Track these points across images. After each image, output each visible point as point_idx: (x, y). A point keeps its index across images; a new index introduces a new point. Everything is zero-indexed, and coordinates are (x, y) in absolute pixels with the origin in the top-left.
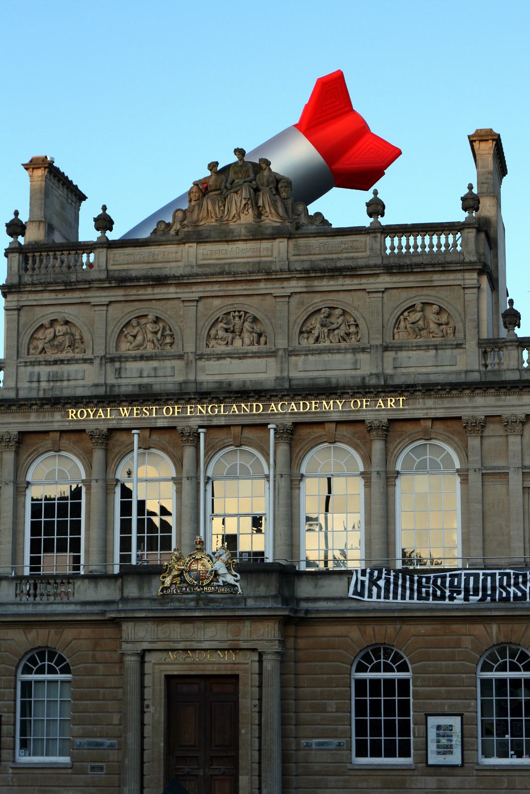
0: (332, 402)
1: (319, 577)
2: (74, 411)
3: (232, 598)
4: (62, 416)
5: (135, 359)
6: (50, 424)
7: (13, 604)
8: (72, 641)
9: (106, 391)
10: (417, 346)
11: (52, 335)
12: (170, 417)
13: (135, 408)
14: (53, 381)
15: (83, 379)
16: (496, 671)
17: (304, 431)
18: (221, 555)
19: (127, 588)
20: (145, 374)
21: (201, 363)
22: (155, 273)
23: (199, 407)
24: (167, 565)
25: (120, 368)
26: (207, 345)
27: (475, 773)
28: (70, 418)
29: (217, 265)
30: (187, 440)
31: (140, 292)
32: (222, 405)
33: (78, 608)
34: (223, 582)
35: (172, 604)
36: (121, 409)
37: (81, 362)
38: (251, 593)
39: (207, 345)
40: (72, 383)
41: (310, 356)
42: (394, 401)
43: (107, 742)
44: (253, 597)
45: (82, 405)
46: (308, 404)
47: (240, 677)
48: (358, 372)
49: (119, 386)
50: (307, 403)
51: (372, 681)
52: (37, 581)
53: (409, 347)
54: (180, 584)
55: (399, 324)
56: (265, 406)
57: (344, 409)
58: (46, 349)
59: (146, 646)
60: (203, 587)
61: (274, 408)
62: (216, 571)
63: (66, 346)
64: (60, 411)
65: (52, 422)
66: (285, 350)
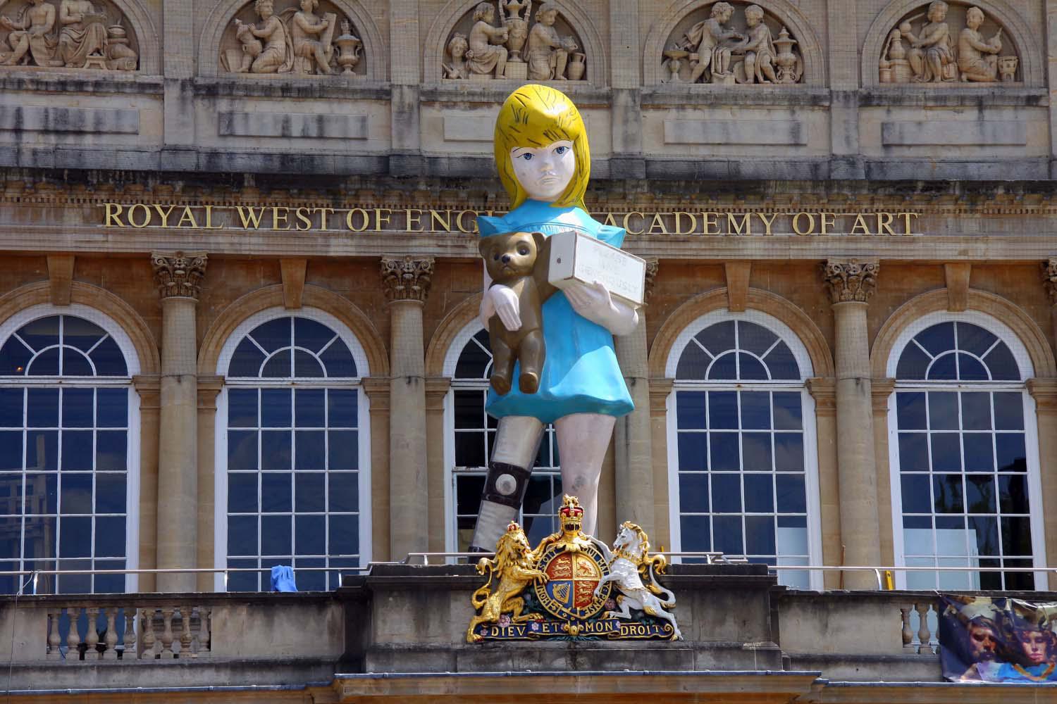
1: (831, 606)
4: (86, 220)
5: (268, 92)
6: (54, 237)
7: (43, 669)
9: (198, 165)
10: (936, 99)
11: (51, 19)
13: (275, 209)
14: (57, 132)
15: (136, 133)
19: (384, 622)
20: (296, 130)
21: (429, 113)
23: (434, 213)
24: (487, 567)
30: (408, 291)
35: (510, 663)
36: (240, 209)
37: (128, 90)
38: (703, 638)
40: (105, 140)
42: (891, 219)
44: (711, 648)
48: (801, 154)
49: (231, 155)
53: (918, 99)
54: (522, 614)
55: (889, 49)
58: (34, 54)
60: (582, 622)
63: (91, 50)
65: (59, 232)
66: (632, 92)
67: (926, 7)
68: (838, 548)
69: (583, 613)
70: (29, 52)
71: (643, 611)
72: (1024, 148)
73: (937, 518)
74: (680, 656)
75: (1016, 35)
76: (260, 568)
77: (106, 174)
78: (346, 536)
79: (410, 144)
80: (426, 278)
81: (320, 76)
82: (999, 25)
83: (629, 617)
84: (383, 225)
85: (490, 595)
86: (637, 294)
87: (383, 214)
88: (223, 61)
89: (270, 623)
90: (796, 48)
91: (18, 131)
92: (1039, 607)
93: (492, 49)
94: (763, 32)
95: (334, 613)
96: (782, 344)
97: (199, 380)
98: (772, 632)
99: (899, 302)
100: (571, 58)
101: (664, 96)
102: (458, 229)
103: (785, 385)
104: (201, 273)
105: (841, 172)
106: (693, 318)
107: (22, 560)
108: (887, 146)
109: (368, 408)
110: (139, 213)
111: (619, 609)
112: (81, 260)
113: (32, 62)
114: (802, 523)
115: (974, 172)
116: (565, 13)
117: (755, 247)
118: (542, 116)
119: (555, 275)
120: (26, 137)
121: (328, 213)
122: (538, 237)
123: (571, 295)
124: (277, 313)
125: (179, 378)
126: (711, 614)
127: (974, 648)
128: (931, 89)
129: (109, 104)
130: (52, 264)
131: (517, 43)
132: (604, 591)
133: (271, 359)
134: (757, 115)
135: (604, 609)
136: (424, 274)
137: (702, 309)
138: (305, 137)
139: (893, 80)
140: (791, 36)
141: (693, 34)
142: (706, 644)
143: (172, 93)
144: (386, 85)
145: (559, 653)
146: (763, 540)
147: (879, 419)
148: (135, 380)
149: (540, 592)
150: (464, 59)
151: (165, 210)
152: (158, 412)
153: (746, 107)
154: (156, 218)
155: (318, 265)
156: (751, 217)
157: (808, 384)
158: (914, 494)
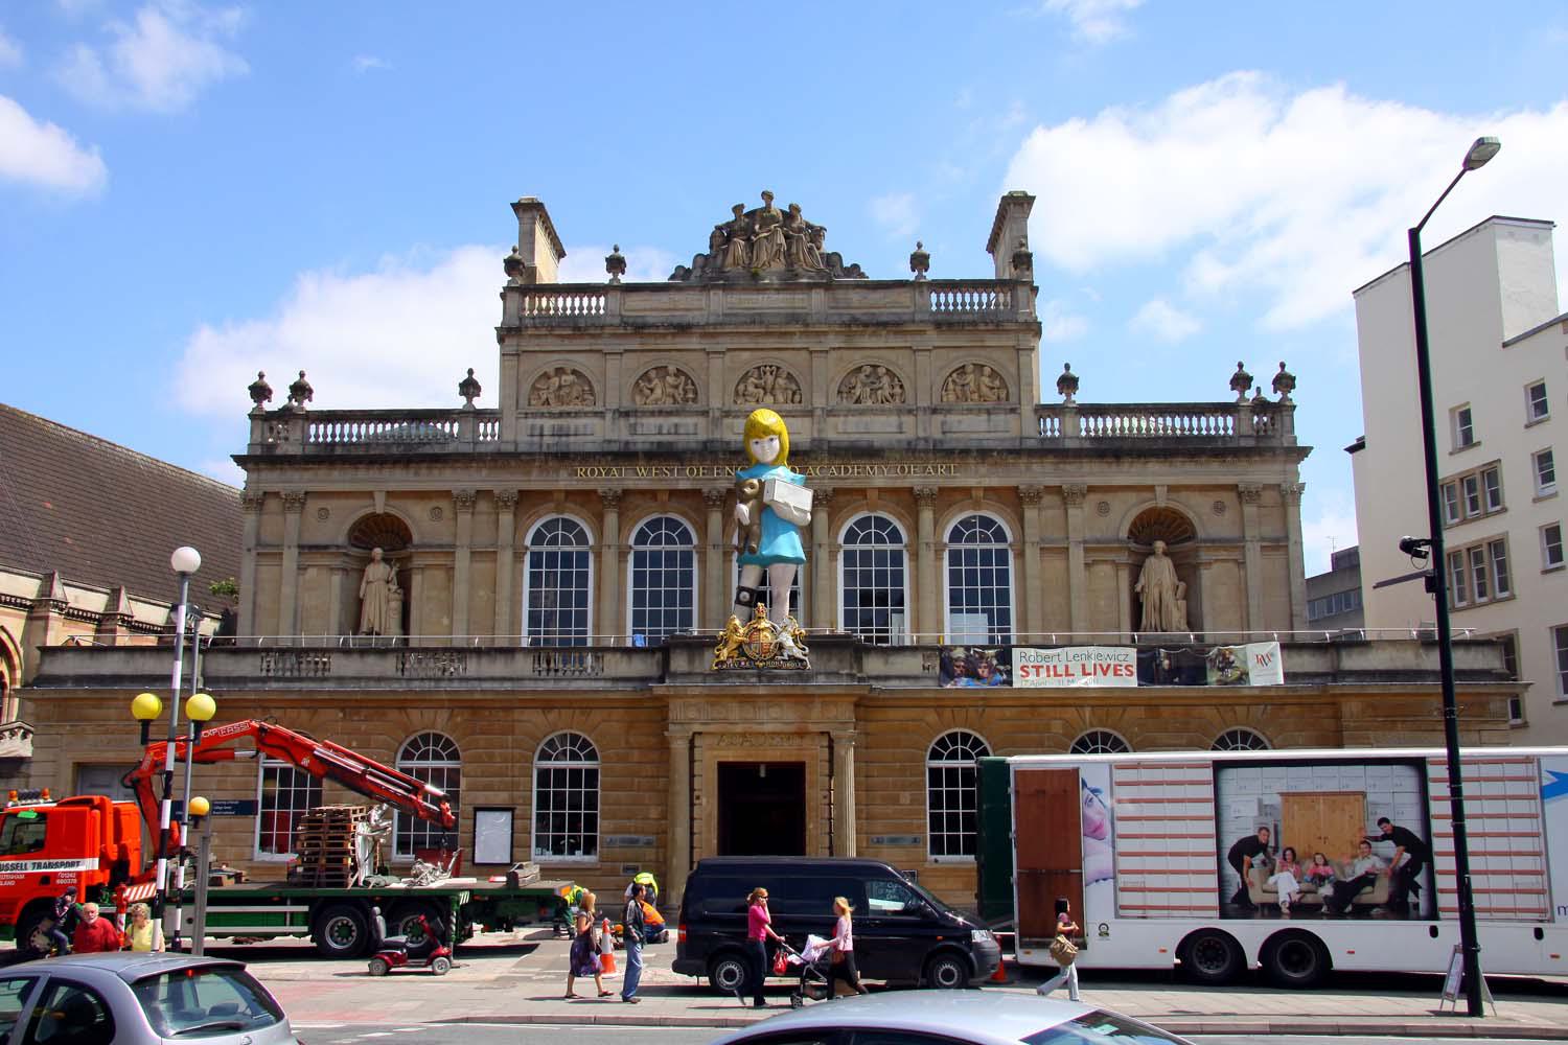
3: (799, 674)
4: (570, 475)
5: (652, 413)
7: (530, 679)
8: (599, 723)
10: (967, 410)
12: (694, 479)
16: (418, 759)
17: (842, 499)
21: (727, 421)
22: (676, 321)
25: (635, 424)
26: (735, 402)
29: (745, 315)
30: (714, 505)
31: (659, 342)
33: (609, 685)
34: (789, 656)
39: (735, 402)
40: (578, 438)
41: (850, 418)
43: (643, 838)
49: (635, 443)
51: (557, 771)
59: (697, 728)
65: (557, 481)
66: (823, 409)
67: (963, 367)
68: (917, 626)
70: (547, 399)
74: (809, 678)
75: (1006, 380)
77: (577, 454)
78: (687, 619)
79: (717, 436)
81: (677, 405)
82: (999, 375)
84: (703, 474)
86: (808, 507)
88: (634, 400)
89: (630, 658)
90: (901, 387)
91: (542, 435)
92: (986, 652)
93: (756, 390)
94: (886, 380)
95: (659, 656)
96: (895, 527)
97: (619, 547)
99: (950, 506)
100: (794, 393)
101: (837, 410)
103: (896, 547)
105: (921, 445)
106: (852, 515)
107: (678, 628)
108: (944, 433)
110: (593, 472)
111: (782, 655)
112: (568, 493)
113: (549, 404)
114: (902, 612)
115: (986, 445)
116: (791, 372)
117: (879, 481)
118: (761, 424)
119: (766, 499)
120: (545, 438)
122: (760, 481)
123: (774, 507)
124: (655, 516)
125: (609, 547)
126: (825, 657)
127: (955, 671)
128: (965, 405)
129: (581, 421)
130: (556, 495)
131: (769, 387)
133: (654, 537)
134: (883, 419)
135: (776, 655)
137: (856, 510)
138: (669, 434)
139: (948, 401)
140: (899, 381)
141: (853, 380)
142: (822, 671)
143: (609, 416)
144: (706, 409)
145: (753, 675)
146: (884, 619)
149: (745, 648)
150: (744, 395)
152: (600, 562)
153: (875, 414)
154: (600, 473)
155: (674, 493)
157: (906, 546)
158: (955, 599)
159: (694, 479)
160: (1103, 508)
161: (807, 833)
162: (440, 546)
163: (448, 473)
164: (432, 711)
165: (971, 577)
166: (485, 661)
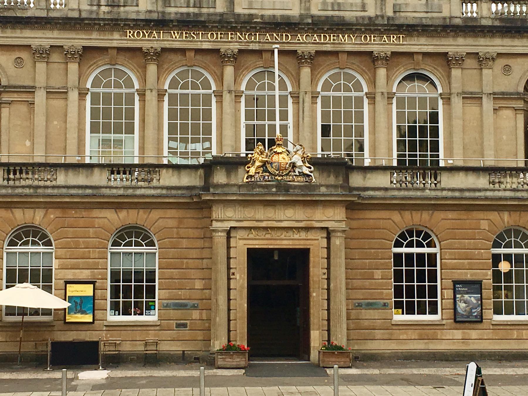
0: (346, 36)
2: (132, 32)
6: (110, 42)
7: (106, 187)
8: (158, 220)
9: (158, 17)
12: (214, 42)
13: (184, 32)
17: (321, 59)
18: (298, 151)
24: (251, 158)
27: (104, 329)
28: (128, 37)
32: (257, 34)
36: (172, 32)
42: (395, 37)
45: (139, 27)
46: (328, 37)
47: (311, 250)
50: (327, 35)
52: (23, 168)
54: (262, 173)
56: (293, 36)
57: (356, 42)
60: (282, 176)
61: (300, 38)
62: (294, 163)
64: (119, 31)
69: (282, 173)
71: (303, 172)
72: (441, 13)
73: (430, 140)
76: (429, 158)
80: (235, 56)
83: (298, 174)
84: (221, 38)
85: (252, 167)
87: (221, 34)
89: (466, 175)
95: (201, 172)
97: (158, 91)
98: (347, 179)
102: (246, 39)
104: (159, 54)
109: (215, 100)
112: (120, 50)
121: (202, 33)
126: (325, 174)
132: (290, 166)
135: (290, 172)
136: (235, 55)
147: (390, 106)
148: (137, 90)
149: (268, 166)
151: (147, 33)
154: (144, 35)
155: (199, 51)
156: (348, 36)
159: (214, 42)
160: (507, 69)
161: (311, 300)
162: (24, 87)
163: (28, 33)
164: (32, 211)
165: (184, 114)
166: (71, 173)
